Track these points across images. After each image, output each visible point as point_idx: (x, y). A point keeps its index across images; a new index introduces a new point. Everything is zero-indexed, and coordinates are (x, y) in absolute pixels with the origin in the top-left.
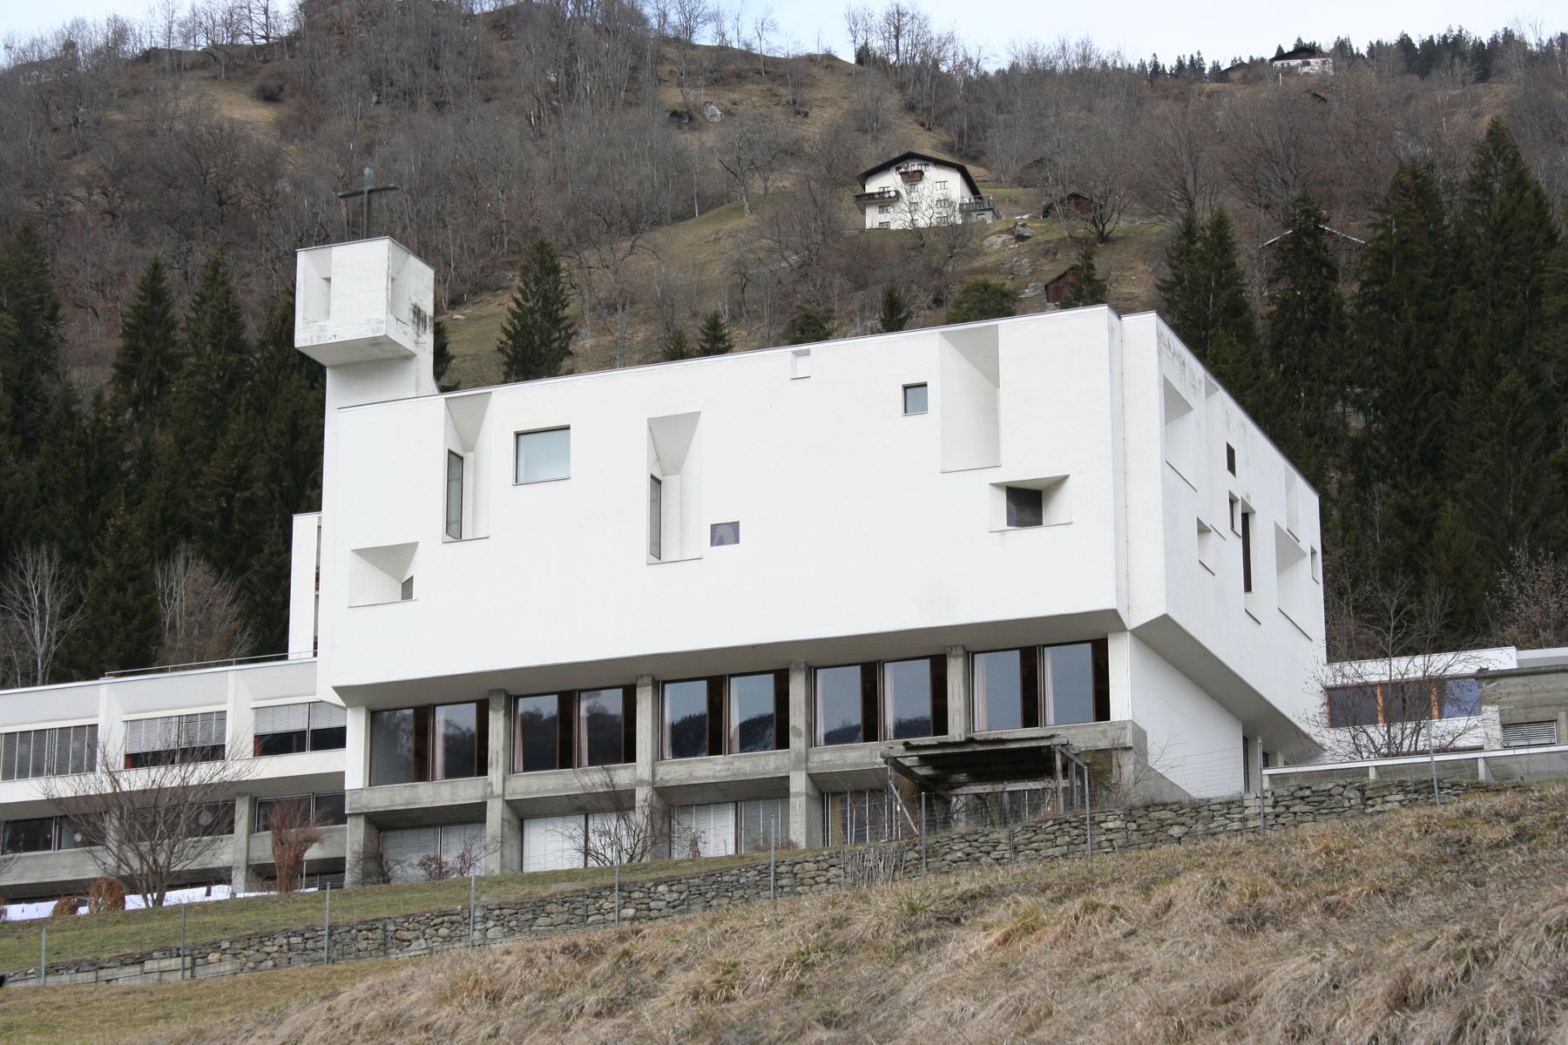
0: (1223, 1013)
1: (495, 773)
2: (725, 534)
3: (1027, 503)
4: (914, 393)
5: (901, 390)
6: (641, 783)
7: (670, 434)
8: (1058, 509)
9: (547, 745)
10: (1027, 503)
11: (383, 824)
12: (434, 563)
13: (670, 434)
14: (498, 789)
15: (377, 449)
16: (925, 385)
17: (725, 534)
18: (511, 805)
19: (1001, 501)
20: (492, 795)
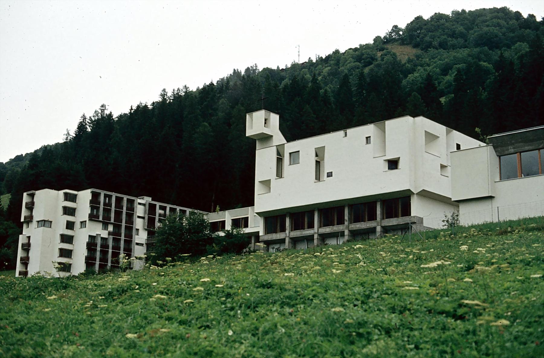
0: (358, 315)
1: (287, 232)
2: (330, 175)
3: (393, 164)
4: (368, 139)
5: (365, 139)
6: (315, 233)
7: (319, 153)
8: (401, 164)
9: (326, 222)
10: (393, 164)
11: (268, 243)
12: (275, 183)
13: (319, 153)
14: (317, 231)
15: (264, 161)
16: (299, 151)
17: (330, 175)
18: (383, 227)
19: (386, 165)
20: (286, 237)
